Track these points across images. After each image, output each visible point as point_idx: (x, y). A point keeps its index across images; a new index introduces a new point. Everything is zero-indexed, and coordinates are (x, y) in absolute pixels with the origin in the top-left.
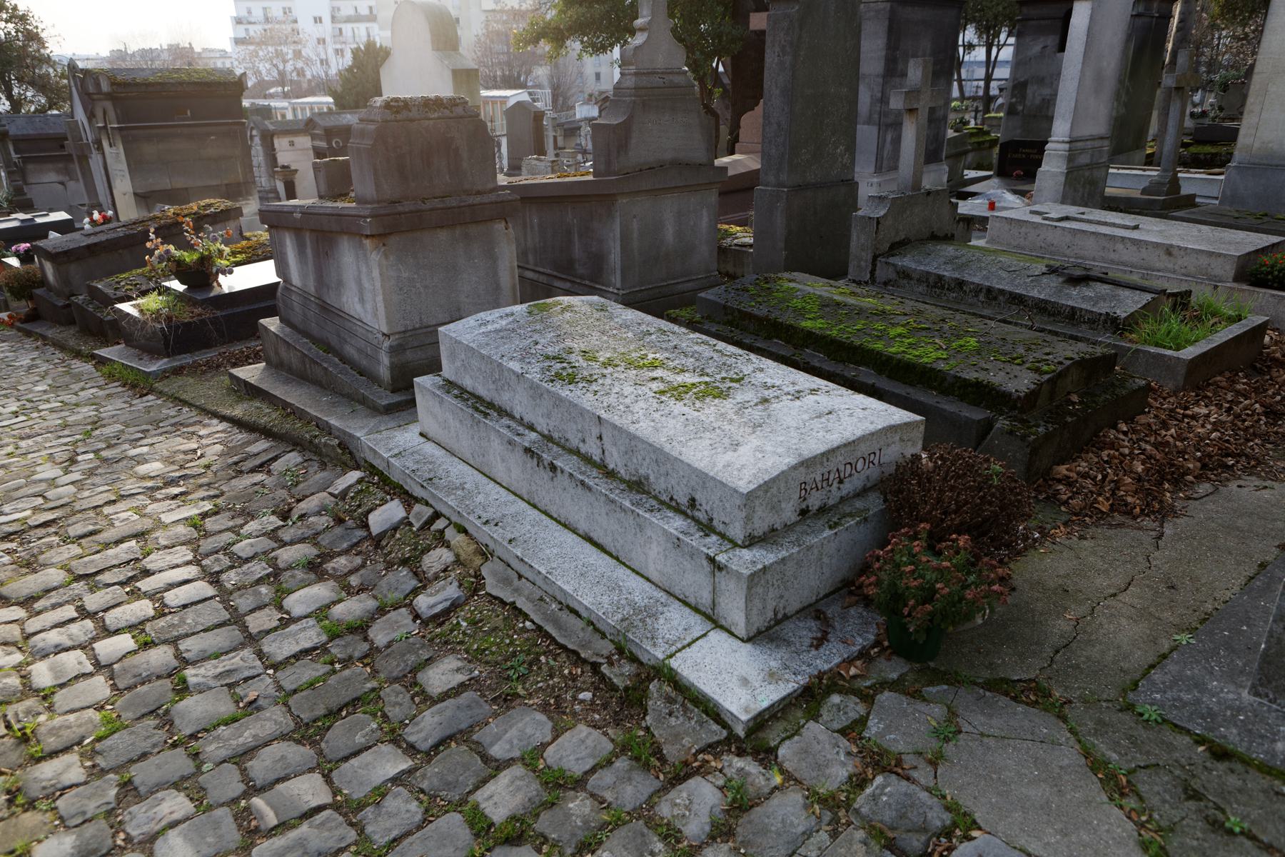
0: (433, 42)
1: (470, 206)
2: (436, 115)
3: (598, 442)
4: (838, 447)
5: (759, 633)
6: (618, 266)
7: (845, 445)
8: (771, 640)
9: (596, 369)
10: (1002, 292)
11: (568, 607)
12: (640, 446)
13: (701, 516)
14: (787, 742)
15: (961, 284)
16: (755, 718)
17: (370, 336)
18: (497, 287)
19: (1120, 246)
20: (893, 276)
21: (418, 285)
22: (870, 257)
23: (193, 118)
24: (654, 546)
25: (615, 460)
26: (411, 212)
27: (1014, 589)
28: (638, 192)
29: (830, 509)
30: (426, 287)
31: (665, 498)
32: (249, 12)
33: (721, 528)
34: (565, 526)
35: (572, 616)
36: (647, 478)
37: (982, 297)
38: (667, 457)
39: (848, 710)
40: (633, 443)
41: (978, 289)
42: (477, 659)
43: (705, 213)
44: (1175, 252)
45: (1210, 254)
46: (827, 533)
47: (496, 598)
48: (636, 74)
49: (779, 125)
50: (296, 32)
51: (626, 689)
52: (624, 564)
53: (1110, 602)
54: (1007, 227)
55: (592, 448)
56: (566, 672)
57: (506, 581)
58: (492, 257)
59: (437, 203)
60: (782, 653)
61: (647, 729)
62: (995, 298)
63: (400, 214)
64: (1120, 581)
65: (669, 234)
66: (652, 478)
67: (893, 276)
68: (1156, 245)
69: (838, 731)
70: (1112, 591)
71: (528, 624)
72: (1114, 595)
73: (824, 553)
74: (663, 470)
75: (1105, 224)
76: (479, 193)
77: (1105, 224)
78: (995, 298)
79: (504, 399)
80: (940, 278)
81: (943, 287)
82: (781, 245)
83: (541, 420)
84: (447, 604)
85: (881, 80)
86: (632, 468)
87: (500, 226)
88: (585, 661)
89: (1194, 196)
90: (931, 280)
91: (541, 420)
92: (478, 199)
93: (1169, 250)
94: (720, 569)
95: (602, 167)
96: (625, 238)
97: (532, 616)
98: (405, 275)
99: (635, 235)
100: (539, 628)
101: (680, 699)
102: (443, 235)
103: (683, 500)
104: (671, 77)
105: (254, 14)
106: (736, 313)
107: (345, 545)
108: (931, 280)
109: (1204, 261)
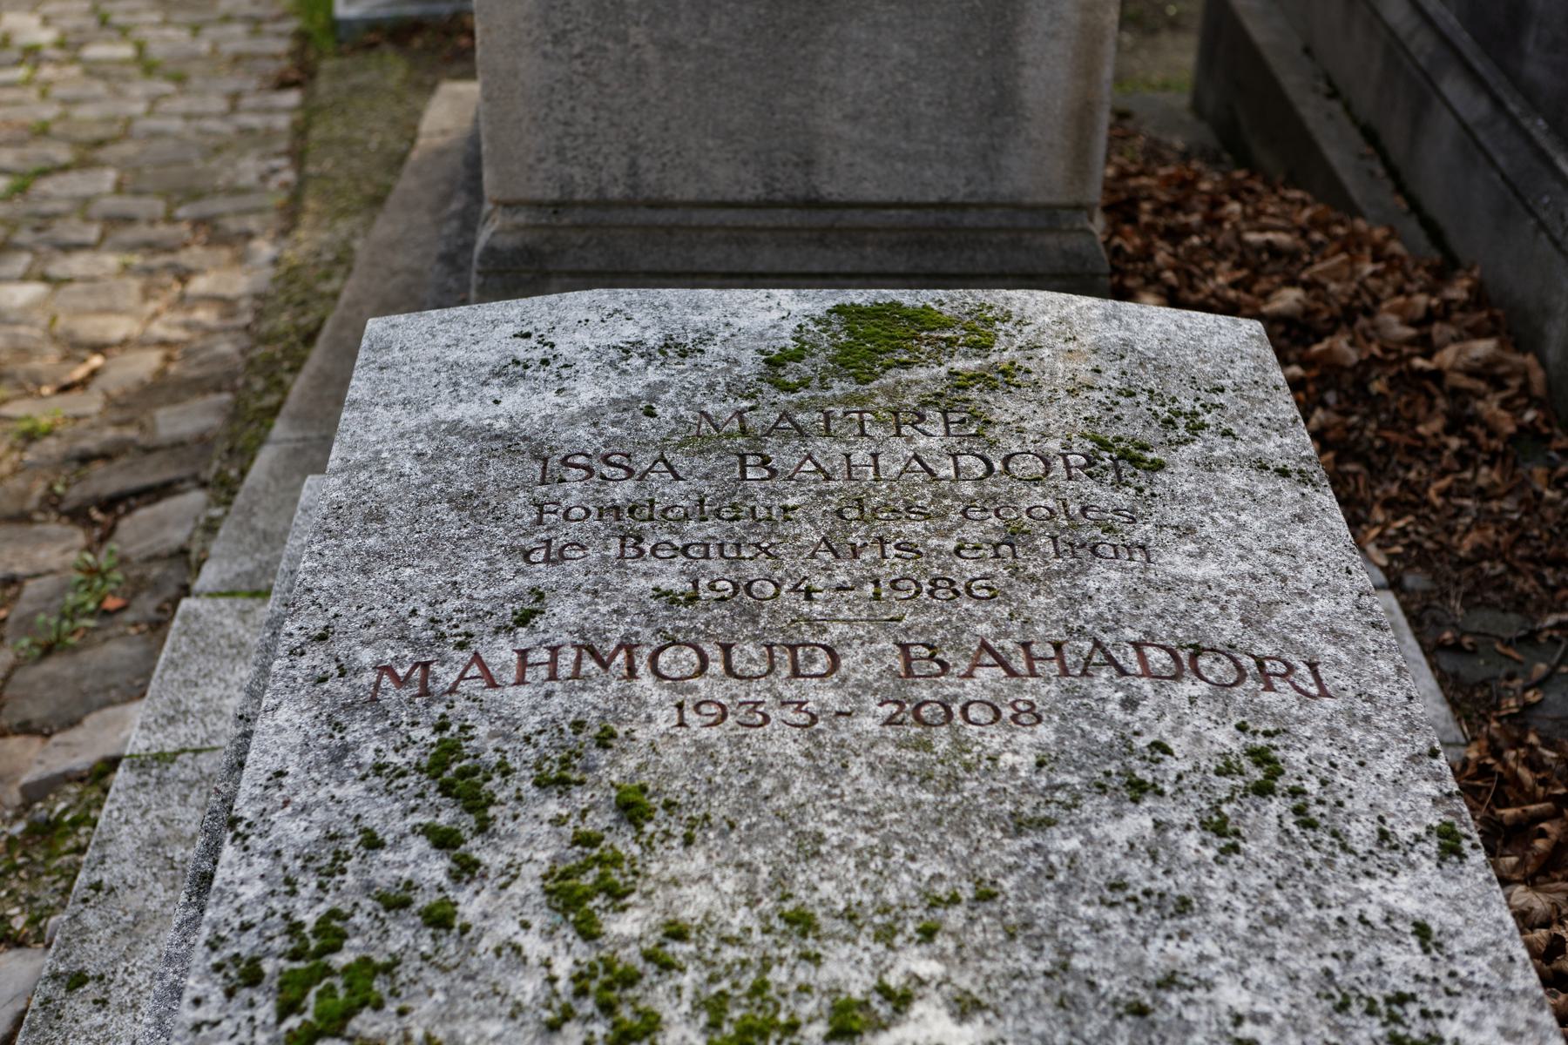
21: (637, 35)
30: (671, 47)
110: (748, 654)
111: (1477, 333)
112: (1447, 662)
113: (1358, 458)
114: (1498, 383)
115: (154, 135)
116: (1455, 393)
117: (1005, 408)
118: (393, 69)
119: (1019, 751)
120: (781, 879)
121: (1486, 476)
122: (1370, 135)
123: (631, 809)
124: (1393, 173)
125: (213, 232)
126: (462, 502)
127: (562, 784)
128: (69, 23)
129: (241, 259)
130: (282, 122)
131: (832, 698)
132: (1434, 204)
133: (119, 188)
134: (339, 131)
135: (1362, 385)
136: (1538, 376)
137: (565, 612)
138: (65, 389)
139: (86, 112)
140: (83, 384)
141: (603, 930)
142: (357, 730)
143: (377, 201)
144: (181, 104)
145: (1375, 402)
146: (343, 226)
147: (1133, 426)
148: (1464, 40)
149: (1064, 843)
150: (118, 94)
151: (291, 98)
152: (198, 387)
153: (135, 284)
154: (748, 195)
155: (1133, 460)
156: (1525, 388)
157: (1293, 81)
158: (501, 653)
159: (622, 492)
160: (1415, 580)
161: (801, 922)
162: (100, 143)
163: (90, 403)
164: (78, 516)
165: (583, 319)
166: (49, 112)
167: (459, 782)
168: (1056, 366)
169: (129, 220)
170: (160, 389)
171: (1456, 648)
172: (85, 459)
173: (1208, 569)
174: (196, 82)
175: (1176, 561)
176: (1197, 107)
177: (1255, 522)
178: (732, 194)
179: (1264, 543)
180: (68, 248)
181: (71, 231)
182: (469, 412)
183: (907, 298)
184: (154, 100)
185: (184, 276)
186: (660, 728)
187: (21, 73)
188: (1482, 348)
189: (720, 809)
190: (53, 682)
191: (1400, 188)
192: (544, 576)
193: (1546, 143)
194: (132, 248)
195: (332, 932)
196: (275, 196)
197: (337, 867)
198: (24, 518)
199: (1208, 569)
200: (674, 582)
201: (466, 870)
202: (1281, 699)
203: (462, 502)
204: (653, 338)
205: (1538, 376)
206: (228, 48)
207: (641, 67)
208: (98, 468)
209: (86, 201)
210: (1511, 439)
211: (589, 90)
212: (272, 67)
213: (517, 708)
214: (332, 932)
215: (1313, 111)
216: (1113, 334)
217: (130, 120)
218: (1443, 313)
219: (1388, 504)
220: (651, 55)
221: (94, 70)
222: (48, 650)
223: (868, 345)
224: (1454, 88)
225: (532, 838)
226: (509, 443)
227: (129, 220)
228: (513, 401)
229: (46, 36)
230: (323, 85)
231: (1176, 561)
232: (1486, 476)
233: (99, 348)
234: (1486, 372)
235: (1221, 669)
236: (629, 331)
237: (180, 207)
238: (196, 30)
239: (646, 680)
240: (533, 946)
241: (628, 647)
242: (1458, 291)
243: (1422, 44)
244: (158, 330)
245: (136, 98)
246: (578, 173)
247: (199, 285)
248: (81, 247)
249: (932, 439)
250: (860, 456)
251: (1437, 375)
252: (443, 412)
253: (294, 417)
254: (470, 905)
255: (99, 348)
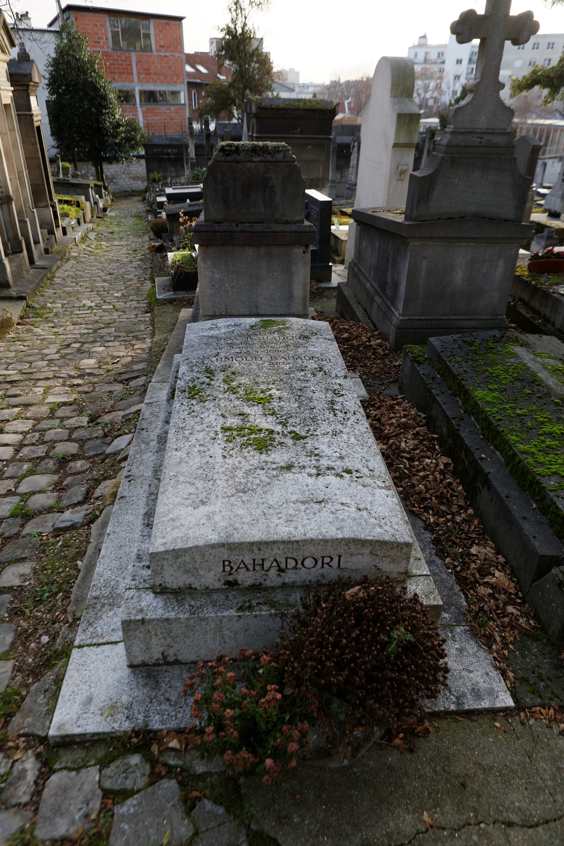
0: (392, 90)
1: (273, 232)
2: (259, 159)
4: (274, 542)
5: (144, 664)
6: (403, 296)
7: (283, 542)
8: (148, 676)
14: (65, 772)
16: (64, 737)
18: (290, 297)
21: (227, 285)
23: (301, 133)
26: (224, 231)
27: (411, 751)
28: (430, 238)
29: (266, 589)
30: (233, 287)
32: (416, 55)
39: (131, 776)
43: (501, 263)
46: (233, 612)
50: (441, 71)
53: (495, 831)
58: (288, 272)
59: (247, 227)
60: (141, 693)
63: (216, 232)
64: (537, 811)
65: (459, 277)
69: (103, 790)
70: (514, 818)
72: (510, 824)
73: (223, 630)
76: (287, 223)
84: (69, 524)
87: (298, 251)
92: (281, 228)
96: (412, 275)
98: (218, 276)
99: (423, 274)
102: (250, 252)
104: (491, 137)
105: (419, 56)
107: (92, 454)
110: (249, 358)
111: (378, 339)
112: (368, 388)
113: (357, 359)
114: (381, 347)
115: (121, 322)
116: (374, 349)
117: (287, 331)
118: (171, 308)
119: (287, 367)
120: (254, 379)
121: (378, 361)
122: (365, 310)
123: (233, 373)
124: (368, 316)
125: (137, 338)
126: (206, 344)
127: (224, 371)
128: (97, 302)
129: (144, 342)
130: (148, 319)
131: (261, 362)
132: (374, 321)
133: (116, 331)
134: (160, 319)
135: (358, 348)
136: (388, 345)
137: (222, 355)
138: (113, 363)
139: (106, 318)
140: (117, 363)
141: (264, 54)
142: (194, 368)
143: (171, 331)
144: (125, 316)
145: (360, 351)
146: (165, 335)
147: (306, 333)
148: (378, 289)
149: (292, 375)
150: (111, 315)
151: (149, 315)
152: (141, 362)
153: (123, 347)
154: (247, 313)
155: (306, 337)
156: (386, 348)
157: (352, 302)
158: (214, 359)
159: (229, 342)
160: (364, 377)
161: (257, 383)
162: (110, 324)
163: (119, 365)
164: (121, 382)
165: (221, 322)
166: (98, 318)
167: (210, 373)
168: (295, 326)
169: (120, 337)
170: (132, 363)
171: (370, 385)
172: (120, 374)
173: (316, 349)
174: (127, 312)
175: (311, 348)
176: (336, 310)
177: (323, 345)
178: (244, 313)
179: (325, 346)
180: (108, 341)
181: (108, 338)
182: (205, 334)
183: (272, 319)
184: (119, 316)
185: (133, 345)
186: (236, 365)
187: (89, 311)
188: (379, 341)
189: (246, 373)
190: (123, 404)
191: (369, 318)
192: (219, 351)
193: (389, 305)
194: (121, 341)
195: (194, 386)
196: (149, 331)
197: (194, 380)
198: (111, 383)
199: (316, 349)
200: (238, 351)
201: (212, 380)
202: (324, 363)
203: (206, 344)
204: (233, 324)
205: (388, 345)
206: (133, 306)
207: (227, 291)
208: (123, 375)
209: (110, 333)
210: (383, 355)
211: (219, 295)
212: (144, 309)
213: (216, 364)
214: (194, 386)
215: (354, 306)
216: (305, 323)
217: (115, 320)
218: (373, 336)
219: (361, 366)
220: (229, 288)
221: (104, 310)
222: (121, 400)
223: (265, 325)
224: (377, 298)
225: (221, 376)
226: (212, 337)
227: (120, 337)
228: (212, 332)
229: (93, 304)
230: (156, 311)
231: (311, 348)
232: (378, 361)
233: (118, 357)
234: (380, 345)
235: (317, 359)
236: (229, 323)
237: (129, 335)
238: (125, 303)
239: (234, 361)
240: (221, 385)
241: (232, 358)
242: (376, 333)
243: (372, 291)
244: (130, 354)
245: (115, 315)
246: (217, 310)
247: (136, 347)
248: (111, 341)
249: (276, 335)
250: (265, 337)
251: (371, 346)
252: (201, 334)
253: (164, 360)
254: (213, 383)
255: (118, 357)
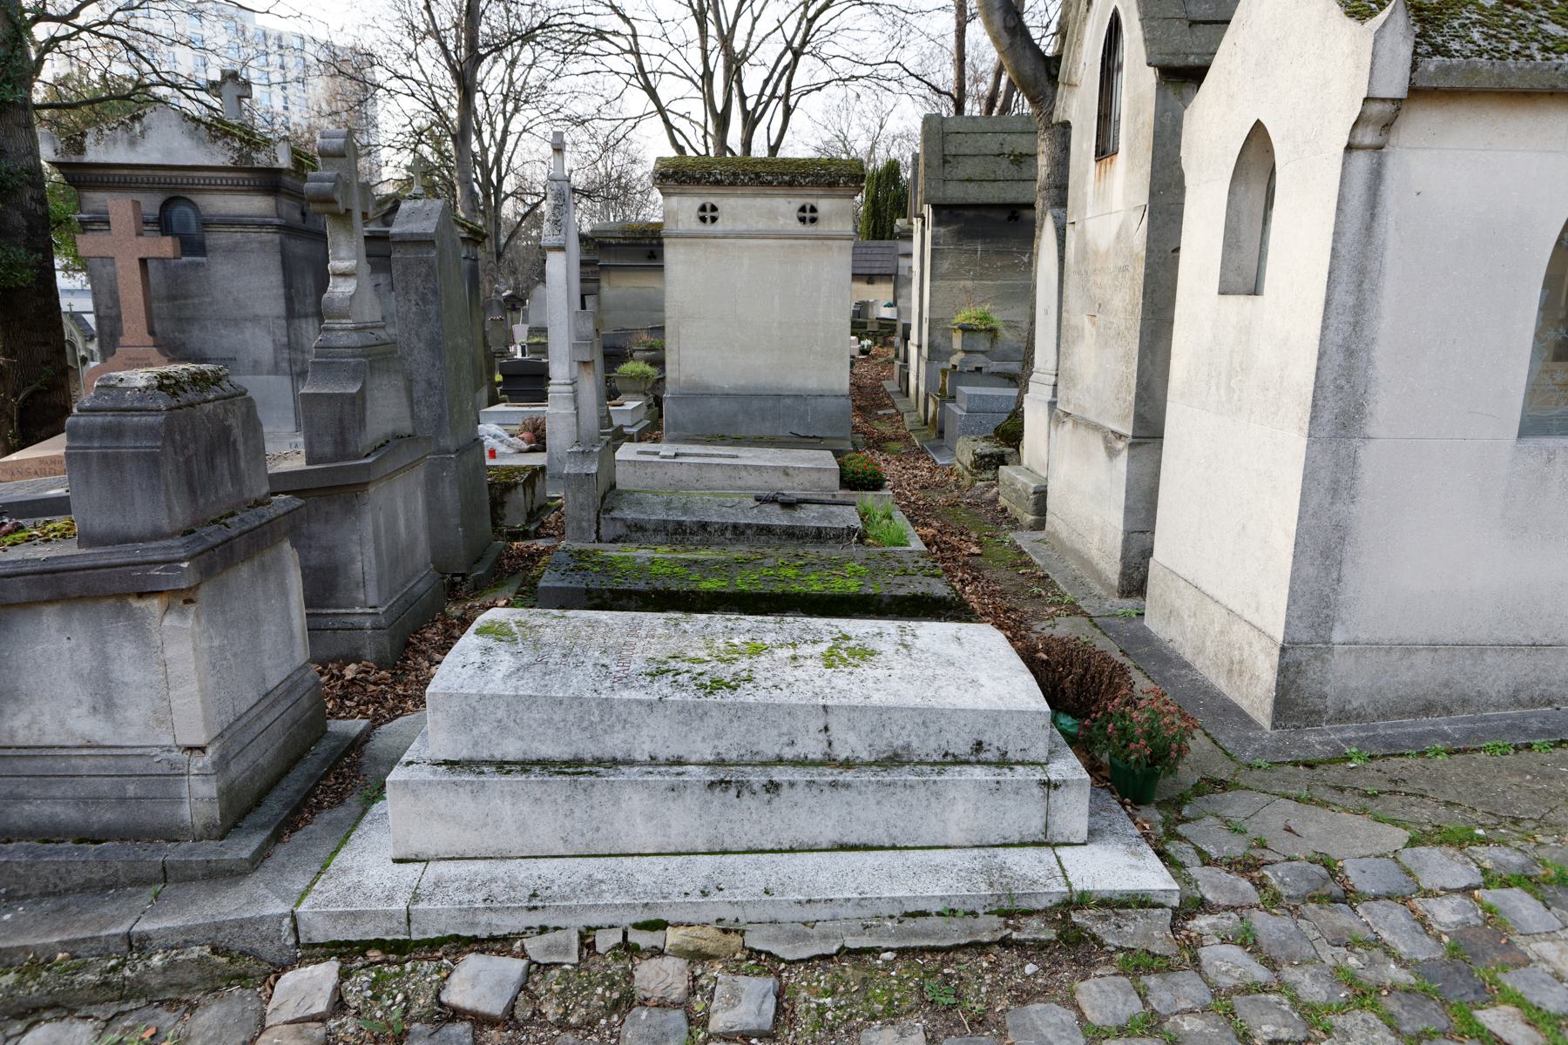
3: (822, 736)
9: (743, 664)
10: (748, 526)
11: (907, 915)
12: (896, 716)
13: (989, 756)
15: (704, 526)
17: (131, 762)
19: (744, 474)
20: (624, 531)
22: (593, 515)
24: (960, 807)
25: (849, 744)
30: (235, 655)
31: (936, 757)
33: (1019, 756)
34: (792, 850)
35: (920, 920)
36: (907, 747)
37: (728, 535)
38: (941, 713)
40: (885, 717)
41: (723, 528)
42: (896, 1016)
44: (791, 472)
45: (819, 470)
47: (811, 959)
48: (356, 329)
49: (429, 383)
51: (1060, 936)
52: (907, 848)
54: (631, 469)
55: (812, 747)
56: (985, 965)
57: (795, 937)
58: (284, 593)
61: (1120, 949)
62: (743, 533)
66: (914, 745)
67: (624, 531)
68: (775, 468)
71: (888, 956)
74: (933, 728)
75: (712, 456)
77: (712, 456)
78: (743, 533)
79: (613, 745)
80: (680, 524)
81: (684, 532)
82: (455, 521)
83: (699, 745)
85: (283, 322)
86: (881, 745)
88: (990, 944)
89: (621, 427)
90: (670, 528)
91: (699, 745)
93: (785, 471)
94: (1056, 787)
95: (328, 450)
97: (884, 945)
100: (901, 952)
101: (1108, 912)
102: (244, 571)
103: (962, 748)
106: (608, 594)
108: (670, 528)
109: (815, 476)
